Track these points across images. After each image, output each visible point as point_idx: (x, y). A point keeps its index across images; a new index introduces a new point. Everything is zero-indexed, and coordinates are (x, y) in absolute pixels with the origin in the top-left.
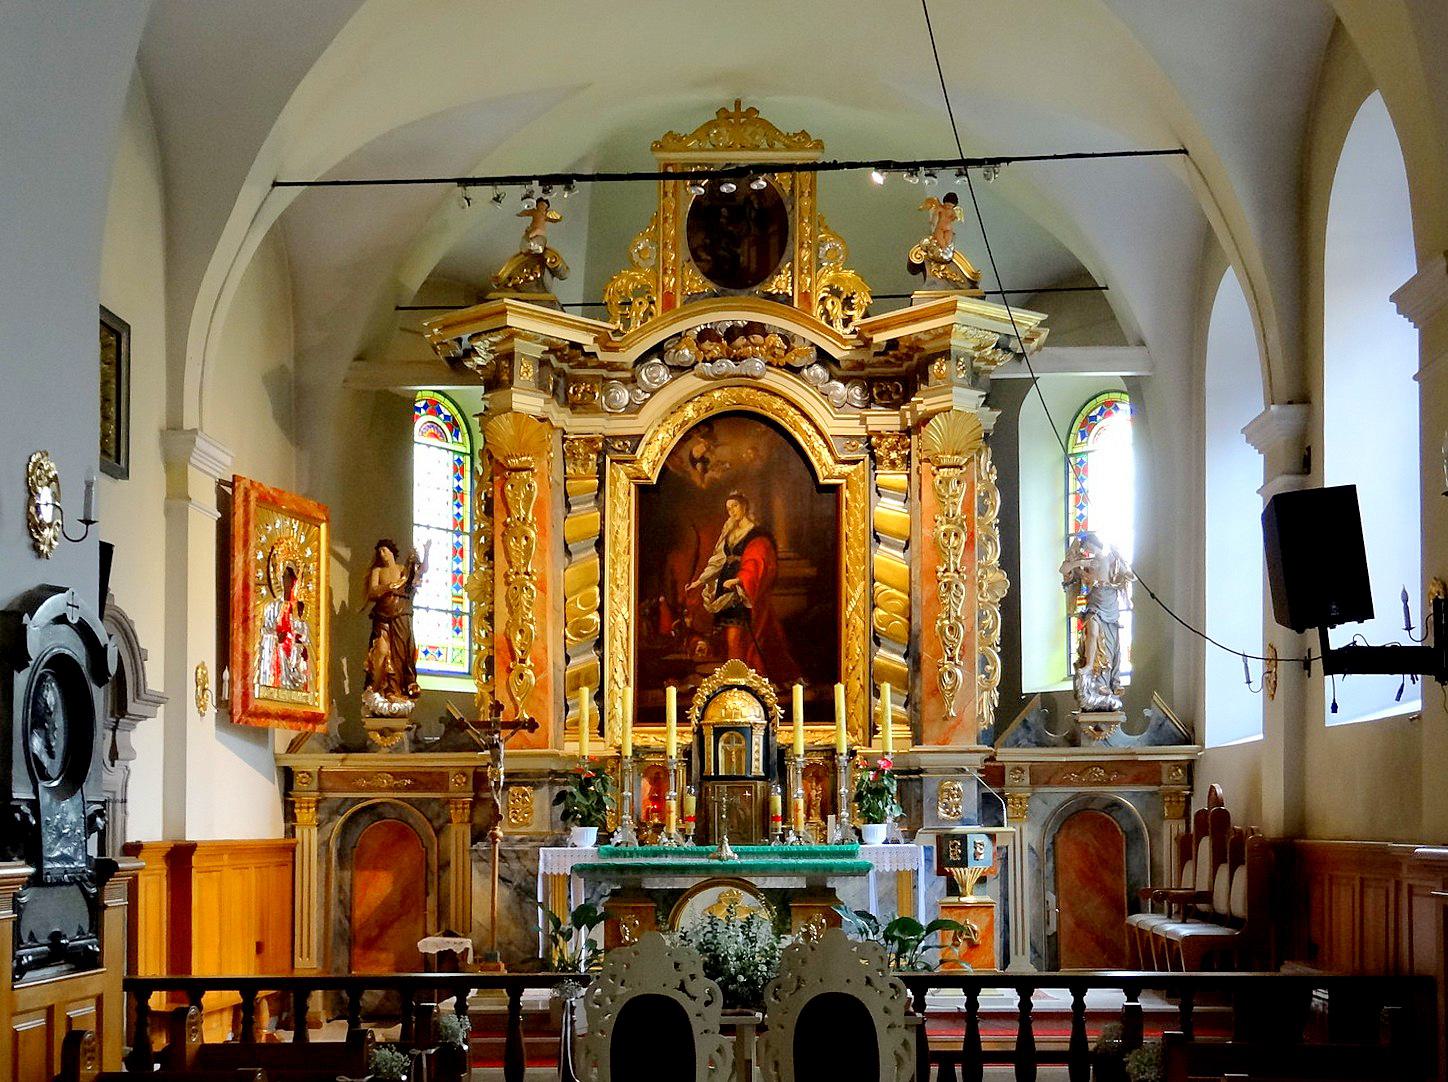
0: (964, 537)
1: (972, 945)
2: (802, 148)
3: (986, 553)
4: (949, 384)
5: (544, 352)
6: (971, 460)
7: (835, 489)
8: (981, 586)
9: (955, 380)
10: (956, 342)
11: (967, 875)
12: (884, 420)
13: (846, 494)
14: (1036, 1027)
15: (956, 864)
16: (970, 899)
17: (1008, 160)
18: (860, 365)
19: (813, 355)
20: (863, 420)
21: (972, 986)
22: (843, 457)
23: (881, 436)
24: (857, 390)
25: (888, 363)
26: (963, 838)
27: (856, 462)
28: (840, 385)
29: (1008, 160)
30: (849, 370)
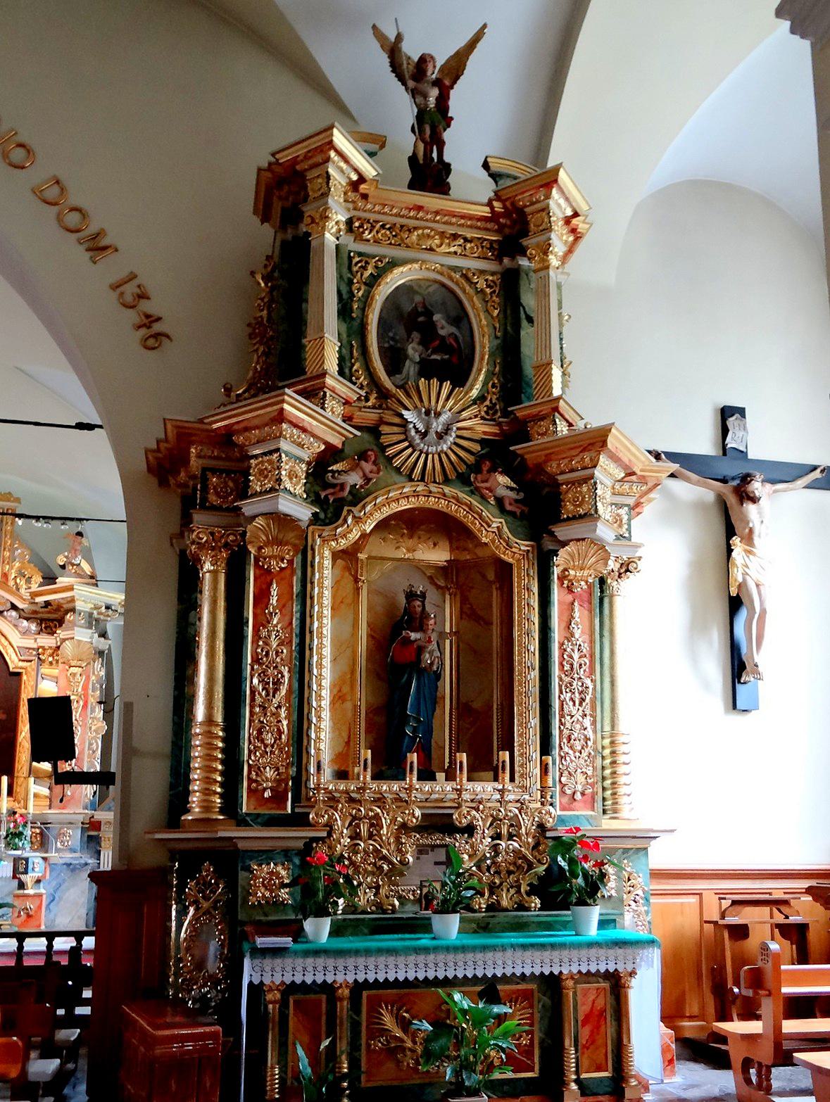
0: (81, 703)
1: (29, 916)
2: (9, 501)
3: (95, 712)
4: (74, 624)
5: (91, 608)
6: (89, 664)
7: (19, 674)
8: (90, 728)
9: (78, 623)
10: (79, 605)
11: (28, 879)
12: (47, 641)
13: (25, 677)
14: (25, 958)
15: (22, 873)
16: (30, 891)
17: (87, 520)
18: (35, 612)
19: (9, 605)
20: (36, 640)
21: (20, 937)
22: (22, 658)
23: (43, 648)
24: (35, 625)
25: (49, 612)
26: (27, 860)
27: (31, 661)
28: (25, 621)
29: (87, 520)
30: (29, 613)
